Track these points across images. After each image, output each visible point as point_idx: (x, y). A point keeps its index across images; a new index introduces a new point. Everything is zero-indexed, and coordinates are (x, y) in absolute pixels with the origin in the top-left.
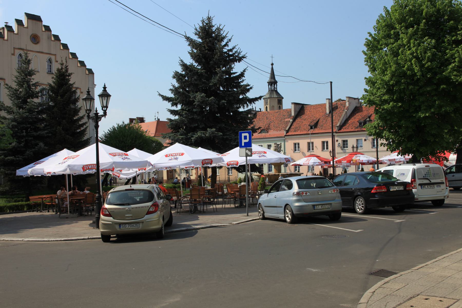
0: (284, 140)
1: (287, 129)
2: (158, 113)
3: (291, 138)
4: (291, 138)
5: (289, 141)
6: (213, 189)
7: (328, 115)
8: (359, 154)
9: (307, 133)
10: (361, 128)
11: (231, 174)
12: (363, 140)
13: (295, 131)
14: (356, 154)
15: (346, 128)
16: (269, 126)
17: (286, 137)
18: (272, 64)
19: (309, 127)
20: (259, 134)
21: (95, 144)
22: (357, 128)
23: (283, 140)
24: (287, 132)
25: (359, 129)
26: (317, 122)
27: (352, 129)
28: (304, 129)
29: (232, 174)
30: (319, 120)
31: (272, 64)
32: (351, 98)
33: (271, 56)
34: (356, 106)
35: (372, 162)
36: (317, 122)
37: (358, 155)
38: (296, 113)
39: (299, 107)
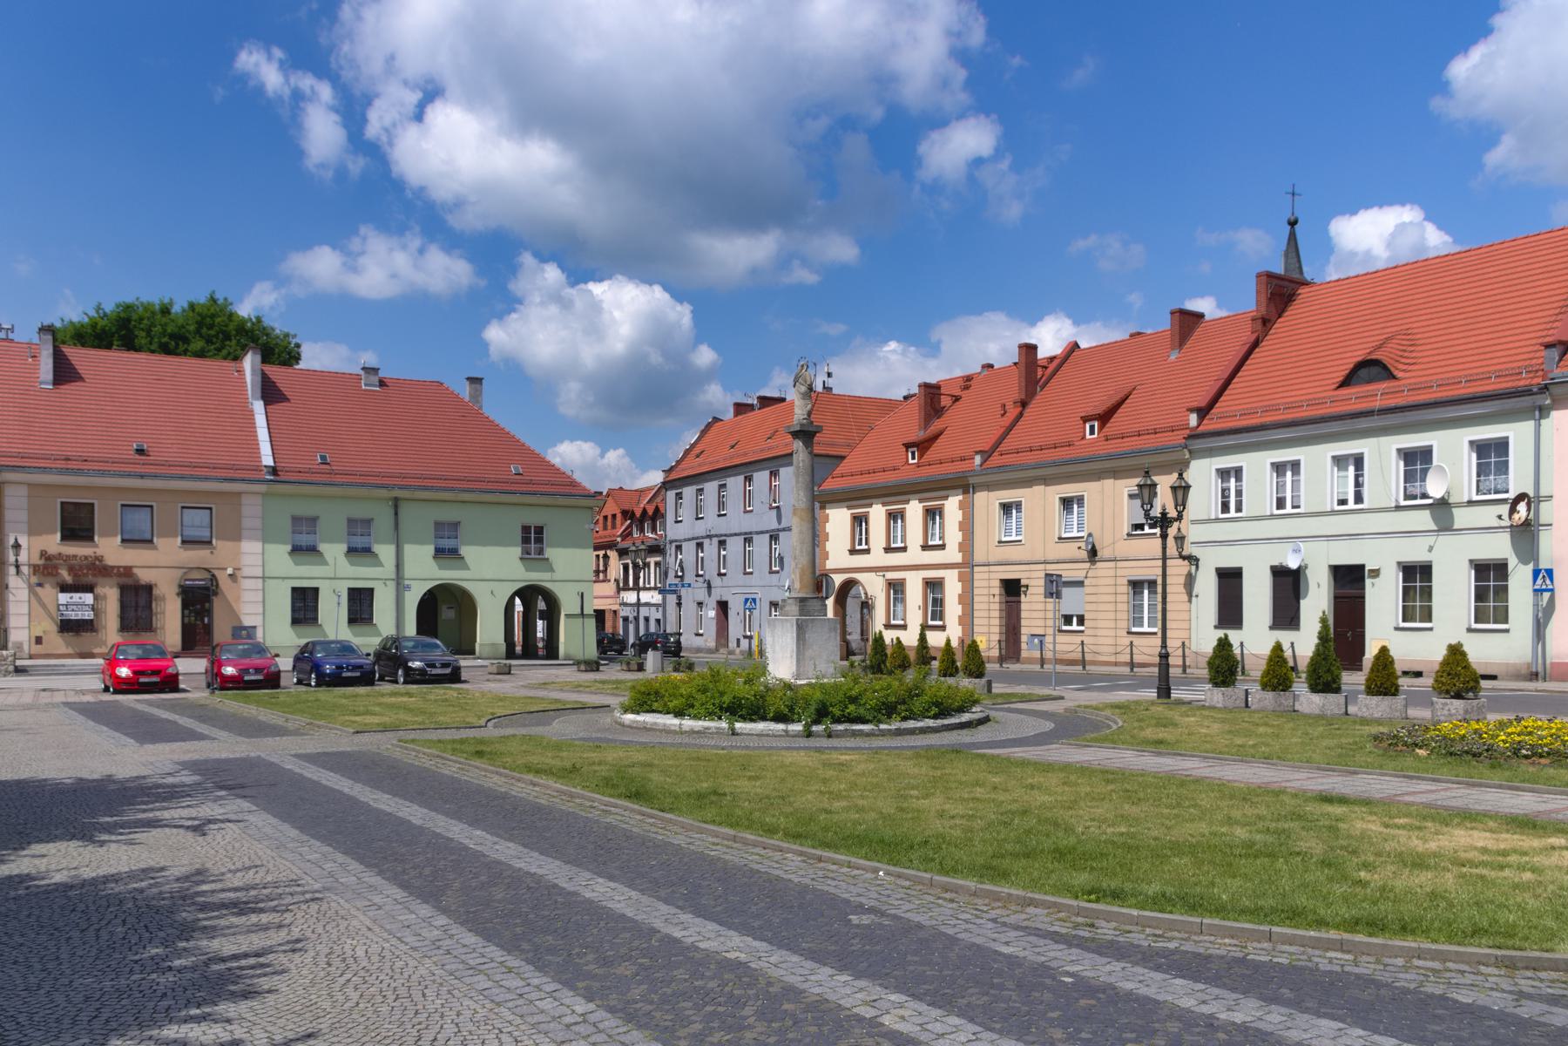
18: (1293, 223)
31: (1293, 223)
33: (1296, 198)
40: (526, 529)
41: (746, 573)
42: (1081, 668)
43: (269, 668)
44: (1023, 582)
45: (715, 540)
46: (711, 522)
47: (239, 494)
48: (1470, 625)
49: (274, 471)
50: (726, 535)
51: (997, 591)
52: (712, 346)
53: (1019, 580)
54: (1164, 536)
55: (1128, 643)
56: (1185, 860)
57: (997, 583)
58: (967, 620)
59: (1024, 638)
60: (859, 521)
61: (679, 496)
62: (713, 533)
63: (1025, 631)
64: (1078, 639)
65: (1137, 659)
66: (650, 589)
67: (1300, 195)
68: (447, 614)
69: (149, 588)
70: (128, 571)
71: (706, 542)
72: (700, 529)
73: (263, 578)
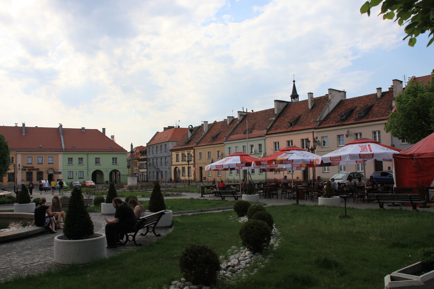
0: (265, 139)
1: (268, 128)
2: (179, 121)
3: (271, 137)
4: (271, 137)
5: (168, 127)
6: (357, 177)
7: (309, 111)
8: (294, 150)
9: (286, 131)
10: (343, 122)
11: (328, 171)
12: (345, 136)
13: (275, 130)
14: (289, 150)
15: (326, 123)
16: (254, 126)
17: (266, 136)
18: (294, 81)
19: (289, 125)
20: (243, 135)
21: (133, 148)
22: (338, 122)
23: (264, 139)
24: (268, 130)
25: (340, 124)
26: (298, 119)
27: (332, 123)
28: (285, 127)
29: (328, 172)
30: (300, 116)
31: (294, 81)
32: (335, 91)
33: (293, 75)
34: (341, 100)
35: (309, 163)
36: (298, 119)
37: (291, 152)
38: (280, 111)
39: (282, 106)
40: (113, 158)
41: (161, 165)
42: (207, 183)
43: (367, 183)
44: (202, 167)
45: (156, 158)
46: (155, 155)
47: (58, 154)
48: (323, 172)
49: (65, 149)
50: (162, 157)
51: (199, 169)
52: (390, 9)
53: (202, 167)
54: (265, 153)
55: (220, 178)
56: (266, 222)
57: (199, 168)
58: (195, 174)
59: (203, 178)
60: (177, 155)
61: (149, 148)
62: (156, 157)
63: (203, 176)
64: (220, 178)
65: (209, 181)
66: (145, 169)
67: (292, 75)
68: (98, 176)
69: (42, 172)
70: (38, 169)
71: (154, 158)
72: (153, 156)
73: (63, 170)
